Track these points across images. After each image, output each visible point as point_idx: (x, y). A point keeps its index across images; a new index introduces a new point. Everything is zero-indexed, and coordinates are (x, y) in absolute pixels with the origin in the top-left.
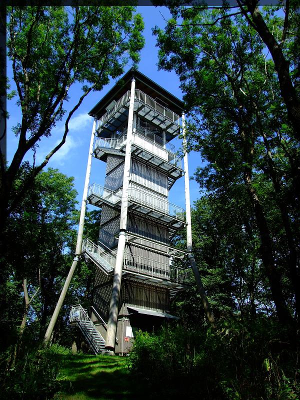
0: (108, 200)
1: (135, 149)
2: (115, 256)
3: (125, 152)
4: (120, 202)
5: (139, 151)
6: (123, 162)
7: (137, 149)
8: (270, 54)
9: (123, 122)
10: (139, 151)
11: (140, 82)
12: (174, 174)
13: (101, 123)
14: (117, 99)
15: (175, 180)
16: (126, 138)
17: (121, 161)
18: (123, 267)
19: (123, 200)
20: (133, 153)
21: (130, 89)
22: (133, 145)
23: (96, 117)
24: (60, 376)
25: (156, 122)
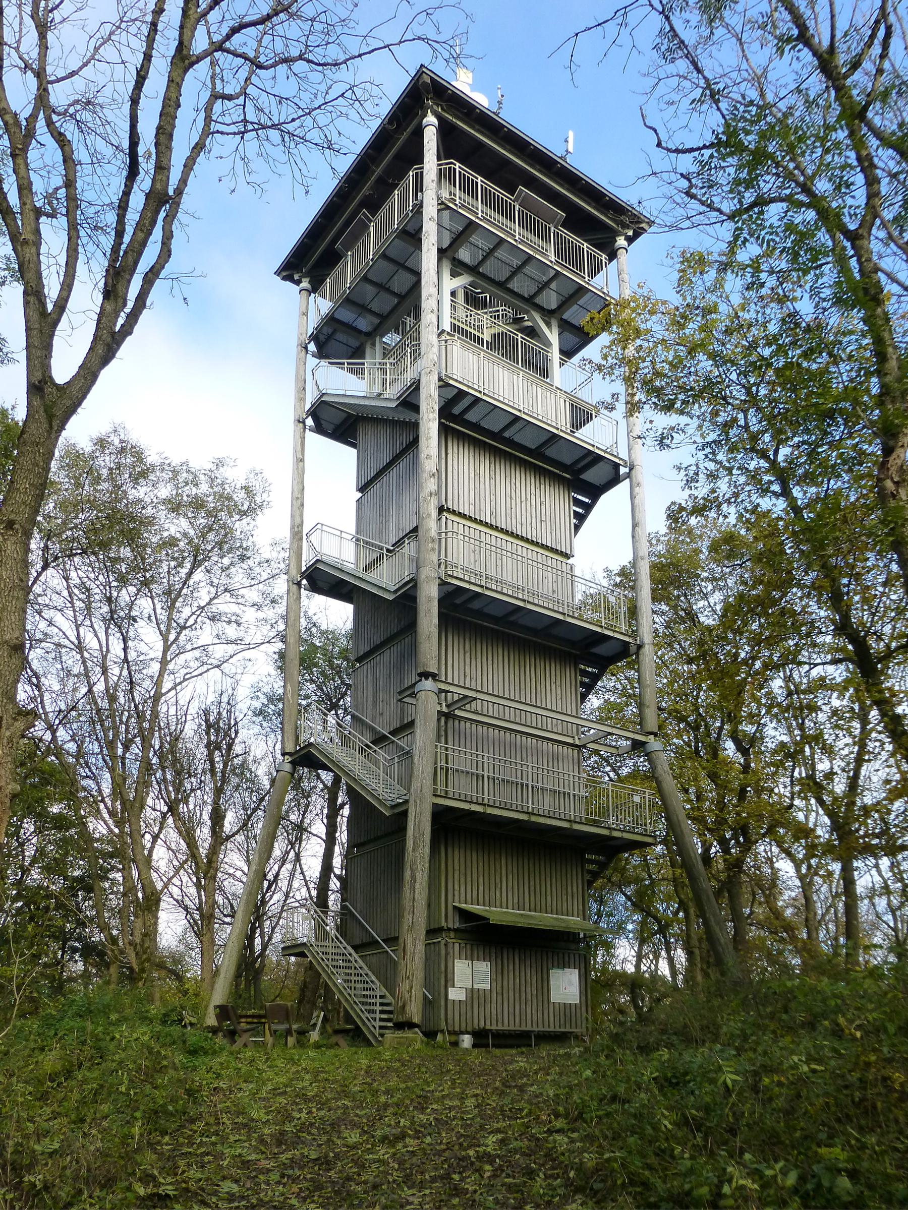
0: (371, 576)
1: (451, 394)
2: (408, 755)
3: (416, 408)
4: (413, 583)
5: (466, 402)
6: (414, 443)
7: (461, 394)
8: (6, 190)
9: (402, 297)
10: (466, 402)
11: (454, 127)
12: (591, 476)
13: (322, 305)
14: (374, 204)
15: (595, 498)
16: (417, 355)
17: (406, 439)
18: (435, 790)
19: (425, 573)
20: (445, 412)
21: (418, 158)
22: (444, 385)
23: (305, 284)
24: (852, 753)
25: (745, 216)
